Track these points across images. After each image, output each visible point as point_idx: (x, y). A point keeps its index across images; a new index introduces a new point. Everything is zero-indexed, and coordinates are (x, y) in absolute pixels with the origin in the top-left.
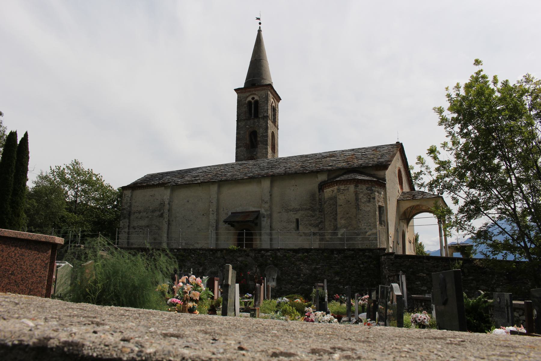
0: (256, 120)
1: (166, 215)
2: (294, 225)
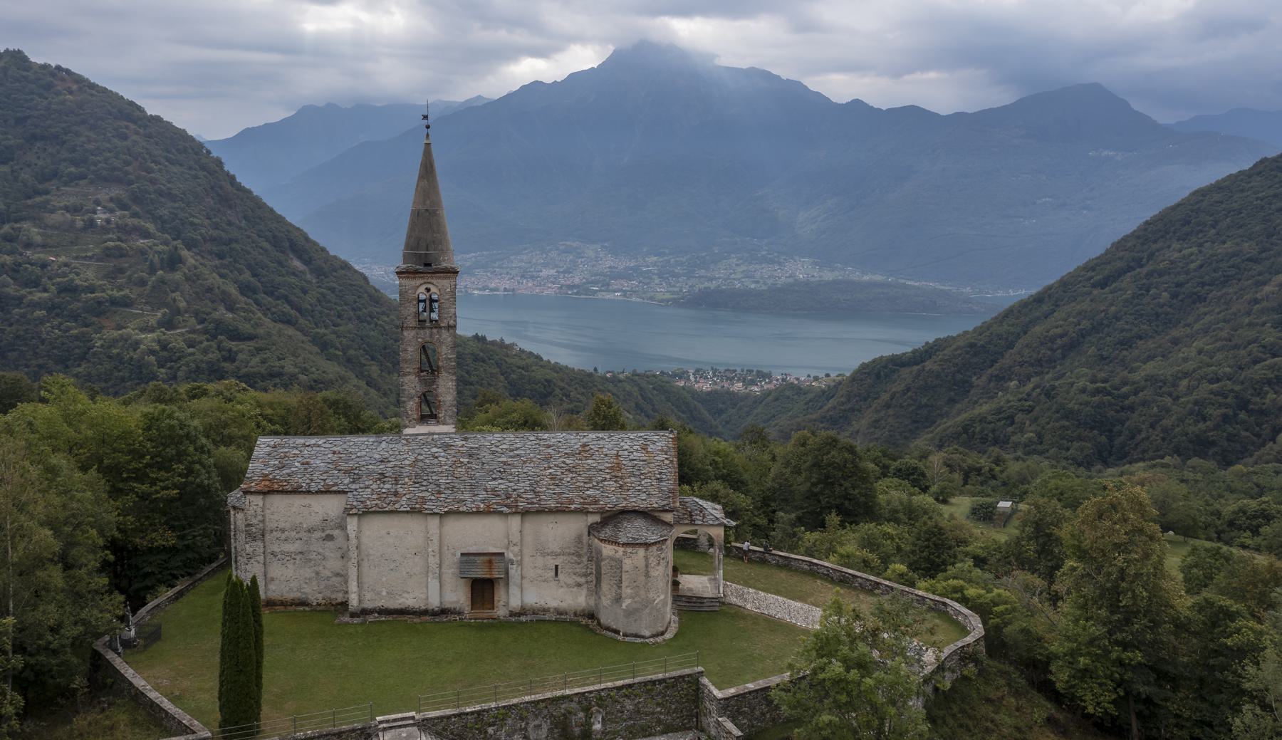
0: (435, 331)
1: (353, 554)
2: (553, 573)
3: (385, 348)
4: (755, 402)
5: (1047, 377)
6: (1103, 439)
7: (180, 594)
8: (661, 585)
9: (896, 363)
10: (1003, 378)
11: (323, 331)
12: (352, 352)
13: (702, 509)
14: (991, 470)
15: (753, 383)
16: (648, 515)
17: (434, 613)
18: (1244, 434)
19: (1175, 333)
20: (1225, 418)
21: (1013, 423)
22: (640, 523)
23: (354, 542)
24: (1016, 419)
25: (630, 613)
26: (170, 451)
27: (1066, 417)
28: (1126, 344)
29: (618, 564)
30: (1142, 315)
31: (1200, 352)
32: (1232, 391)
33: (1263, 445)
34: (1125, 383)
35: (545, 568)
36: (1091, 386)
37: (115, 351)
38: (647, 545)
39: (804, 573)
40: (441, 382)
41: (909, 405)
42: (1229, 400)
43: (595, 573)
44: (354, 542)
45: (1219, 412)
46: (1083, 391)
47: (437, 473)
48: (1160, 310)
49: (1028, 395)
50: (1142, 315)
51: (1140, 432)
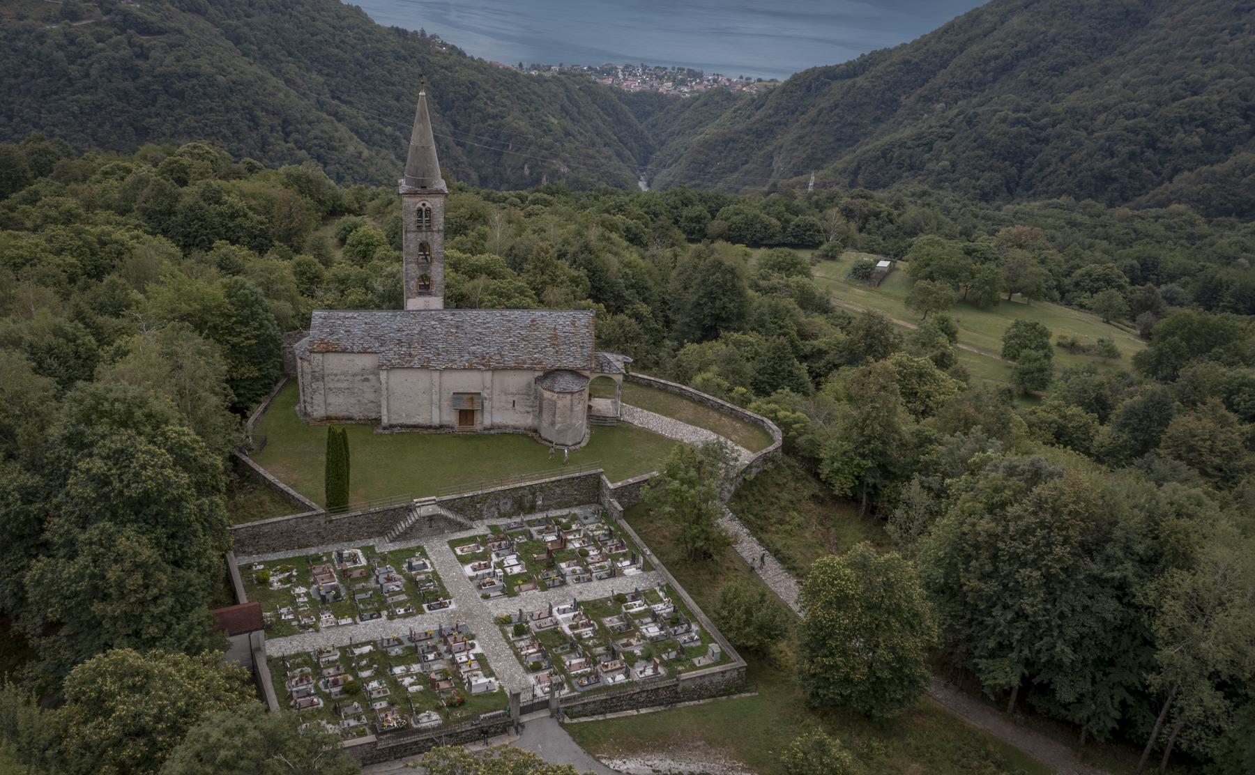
1: (384, 393)
3: (302, 43)
4: (683, 106)
5: (975, 101)
6: (1014, 171)
7: (266, 408)
8: (580, 415)
9: (828, 75)
10: (930, 100)
11: (235, 22)
12: (267, 47)
13: (609, 362)
14: (890, 214)
15: (683, 82)
16: (575, 373)
17: (436, 428)
18: (1146, 171)
19: (1108, 61)
20: (1132, 156)
21: (930, 150)
22: (568, 378)
23: (384, 386)
24: (935, 146)
25: (560, 432)
26: (247, 312)
27: (982, 147)
28: (1058, 70)
29: (554, 404)
30: (1080, 40)
31: (1125, 85)
32: (1144, 128)
33: (1161, 183)
34: (1046, 115)
35: (507, 402)
36: (1013, 116)
37: (20, 44)
38: (572, 393)
39: (676, 394)
40: (433, 268)
41: (835, 123)
42: (1140, 137)
43: (538, 407)
44: (384, 386)
45: (1127, 149)
46: (1004, 120)
47: (436, 340)
48: (1099, 35)
49: (951, 121)
50: (1080, 40)
51: (1049, 165)
